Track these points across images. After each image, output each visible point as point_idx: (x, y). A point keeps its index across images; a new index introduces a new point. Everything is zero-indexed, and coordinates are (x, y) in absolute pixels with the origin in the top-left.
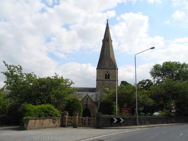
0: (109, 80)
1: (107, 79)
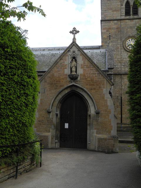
0: (136, 17)
1: (132, 17)
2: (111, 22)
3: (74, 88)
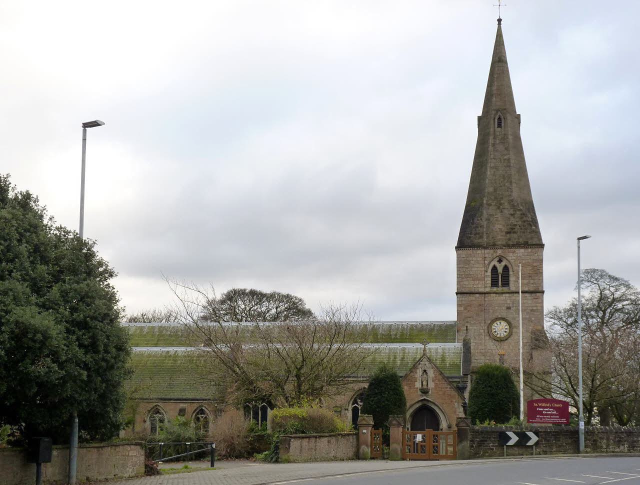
0: (506, 289)
1: (500, 289)
2: (471, 295)
3: (425, 402)
